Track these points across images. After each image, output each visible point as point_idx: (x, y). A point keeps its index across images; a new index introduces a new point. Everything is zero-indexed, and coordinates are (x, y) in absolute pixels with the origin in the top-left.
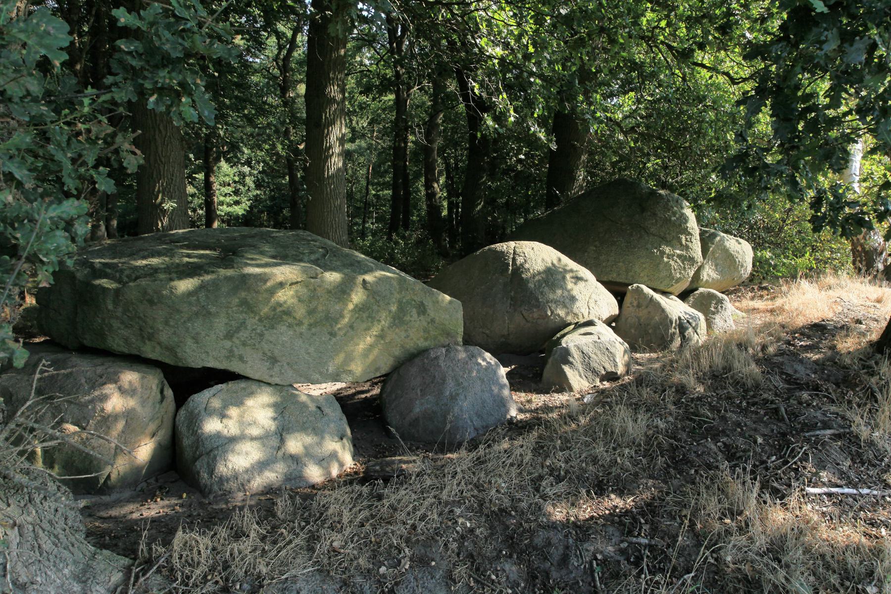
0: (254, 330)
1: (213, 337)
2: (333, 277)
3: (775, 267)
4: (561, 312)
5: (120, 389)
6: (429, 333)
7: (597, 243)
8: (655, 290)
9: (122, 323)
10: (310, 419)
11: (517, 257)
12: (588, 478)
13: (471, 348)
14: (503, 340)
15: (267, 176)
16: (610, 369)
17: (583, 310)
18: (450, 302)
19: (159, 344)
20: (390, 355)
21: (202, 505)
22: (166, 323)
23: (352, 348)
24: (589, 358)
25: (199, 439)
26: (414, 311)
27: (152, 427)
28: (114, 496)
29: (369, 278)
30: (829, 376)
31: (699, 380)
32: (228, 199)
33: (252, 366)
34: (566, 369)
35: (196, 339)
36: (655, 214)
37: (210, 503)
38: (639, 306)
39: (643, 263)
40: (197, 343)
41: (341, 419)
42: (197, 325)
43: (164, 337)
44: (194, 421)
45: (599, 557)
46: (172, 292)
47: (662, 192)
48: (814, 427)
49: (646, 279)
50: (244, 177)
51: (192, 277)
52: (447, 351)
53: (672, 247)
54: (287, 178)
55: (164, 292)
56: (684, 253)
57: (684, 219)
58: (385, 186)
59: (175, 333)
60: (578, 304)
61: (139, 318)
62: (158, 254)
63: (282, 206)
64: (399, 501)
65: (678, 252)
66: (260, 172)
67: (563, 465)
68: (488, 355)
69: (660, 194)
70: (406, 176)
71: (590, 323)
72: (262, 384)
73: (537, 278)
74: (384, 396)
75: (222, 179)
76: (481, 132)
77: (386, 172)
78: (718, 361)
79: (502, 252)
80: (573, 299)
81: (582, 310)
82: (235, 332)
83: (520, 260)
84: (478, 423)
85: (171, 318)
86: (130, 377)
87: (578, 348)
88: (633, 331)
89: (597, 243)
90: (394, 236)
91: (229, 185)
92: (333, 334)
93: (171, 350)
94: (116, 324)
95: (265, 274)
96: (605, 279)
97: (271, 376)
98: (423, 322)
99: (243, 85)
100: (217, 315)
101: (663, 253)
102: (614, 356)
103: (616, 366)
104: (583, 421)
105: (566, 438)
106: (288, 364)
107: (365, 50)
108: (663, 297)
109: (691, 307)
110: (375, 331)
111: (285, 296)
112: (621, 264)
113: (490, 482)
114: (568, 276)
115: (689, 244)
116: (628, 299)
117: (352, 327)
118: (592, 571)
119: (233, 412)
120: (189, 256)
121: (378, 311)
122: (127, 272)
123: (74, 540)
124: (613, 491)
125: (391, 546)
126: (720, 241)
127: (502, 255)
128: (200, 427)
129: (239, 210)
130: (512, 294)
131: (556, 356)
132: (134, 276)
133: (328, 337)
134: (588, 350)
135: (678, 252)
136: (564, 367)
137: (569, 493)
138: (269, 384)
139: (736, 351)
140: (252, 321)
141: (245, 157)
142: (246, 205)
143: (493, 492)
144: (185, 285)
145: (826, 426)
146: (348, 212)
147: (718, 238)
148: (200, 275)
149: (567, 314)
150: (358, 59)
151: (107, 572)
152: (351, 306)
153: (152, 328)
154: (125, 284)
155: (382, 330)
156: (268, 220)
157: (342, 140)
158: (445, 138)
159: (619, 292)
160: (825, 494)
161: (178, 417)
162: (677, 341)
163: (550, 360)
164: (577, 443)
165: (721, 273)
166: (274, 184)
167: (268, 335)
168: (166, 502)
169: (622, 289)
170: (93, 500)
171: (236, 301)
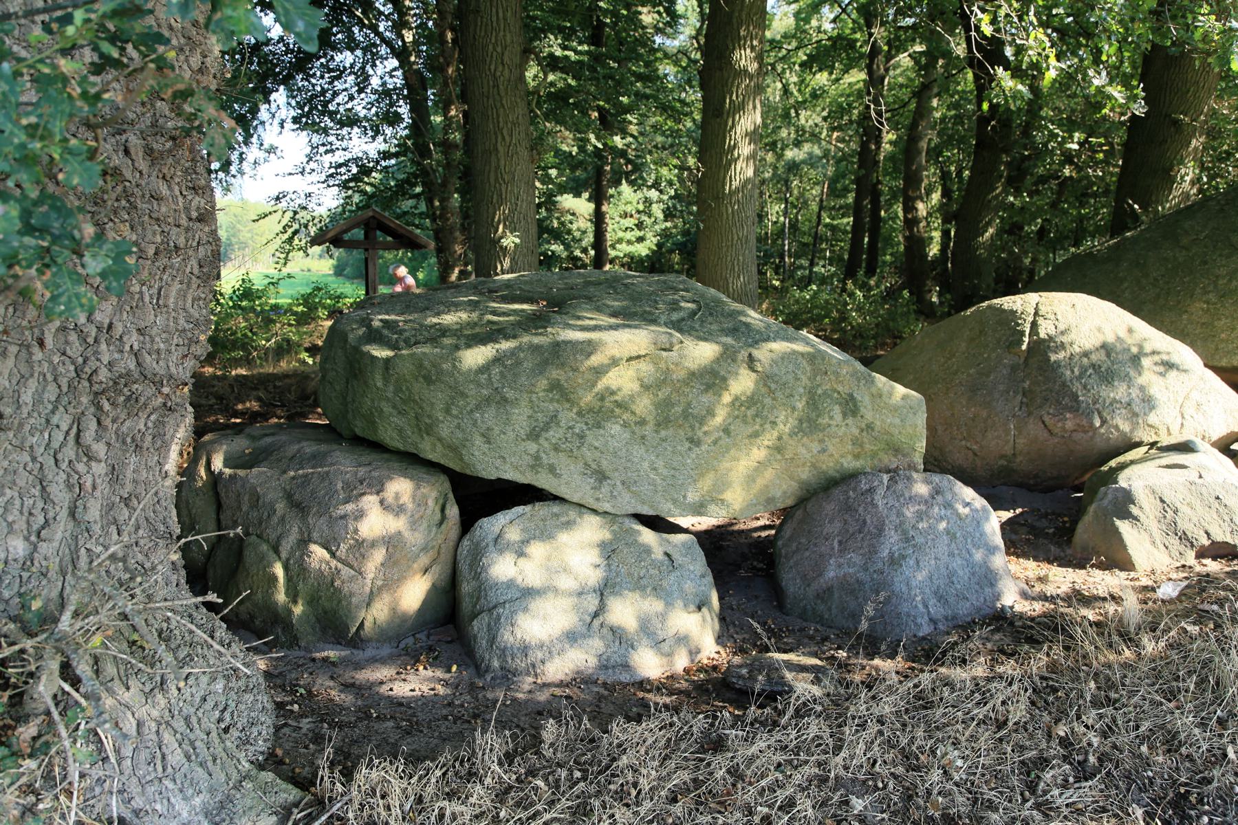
0: (570, 428)
2: (702, 352)
4: (1125, 427)
5: (382, 502)
6: (861, 446)
7: (1212, 297)
9: (394, 407)
10: (652, 572)
11: (1040, 321)
12: (1151, 780)
13: (936, 478)
18: (904, 397)
19: (440, 440)
20: (791, 478)
21: (472, 688)
22: (447, 411)
23: (728, 465)
25: (482, 586)
26: (837, 409)
27: (424, 560)
28: (369, 652)
32: (629, 235)
34: (1123, 526)
37: (483, 688)
40: (489, 442)
41: (703, 576)
42: (489, 417)
43: (445, 430)
46: (454, 366)
51: (485, 344)
55: (444, 366)
58: (844, 211)
59: (458, 426)
61: (414, 401)
64: (751, 760)
67: (1096, 741)
68: (968, 493)
70: (875, 195)
71: (1185, 447)
72: (584, 510)
74: (780, 543)
75: (622, 208)
76: (990, 102)
79: (1013, 312)
80: (1149, 402)
82: (542, 430)
83: (1045, 329)
84: (936, 610)
85: (453, 404)
86: (400, 487)
89: (1212, 297)
92: (695, 442)
93: (454, 449)
94: (387, 409)
96: (1216, 364)
99: (651, 77)
104: (1150, 646)
105: (1108, 679)
106: (623, 483)
107: (826, 10)
110: (769, 438)
111: (622, 380)
113: (933, 752)
114: (1146, 362)
117: (726, 431)
119: (537, 550)
120: (494, 313)
121: (773, 407)
123: (219, 750)
127: (1011, 317)
128: (485, 569)
129: (642, 250)
131: (1106, 502)
132: (413, 340)
133: (687, 445)
136: (1118, 523)
137: (1104, 810)
140: (567, 416)
142: (651, 242)
143: (936, 775)
144: (475, 357)
146: (789, 250)
148: (496, 341)
150: (814, 23)
151: (253, 813)
153: (429, 417)
155: (780, 438)
156: (681, 263)
157: (754, 136)
161: (460, 550)
164: (1132, 694)
167: (590, 437)
168: (429, 673)
170: (343, 653)
171: (543, 383)
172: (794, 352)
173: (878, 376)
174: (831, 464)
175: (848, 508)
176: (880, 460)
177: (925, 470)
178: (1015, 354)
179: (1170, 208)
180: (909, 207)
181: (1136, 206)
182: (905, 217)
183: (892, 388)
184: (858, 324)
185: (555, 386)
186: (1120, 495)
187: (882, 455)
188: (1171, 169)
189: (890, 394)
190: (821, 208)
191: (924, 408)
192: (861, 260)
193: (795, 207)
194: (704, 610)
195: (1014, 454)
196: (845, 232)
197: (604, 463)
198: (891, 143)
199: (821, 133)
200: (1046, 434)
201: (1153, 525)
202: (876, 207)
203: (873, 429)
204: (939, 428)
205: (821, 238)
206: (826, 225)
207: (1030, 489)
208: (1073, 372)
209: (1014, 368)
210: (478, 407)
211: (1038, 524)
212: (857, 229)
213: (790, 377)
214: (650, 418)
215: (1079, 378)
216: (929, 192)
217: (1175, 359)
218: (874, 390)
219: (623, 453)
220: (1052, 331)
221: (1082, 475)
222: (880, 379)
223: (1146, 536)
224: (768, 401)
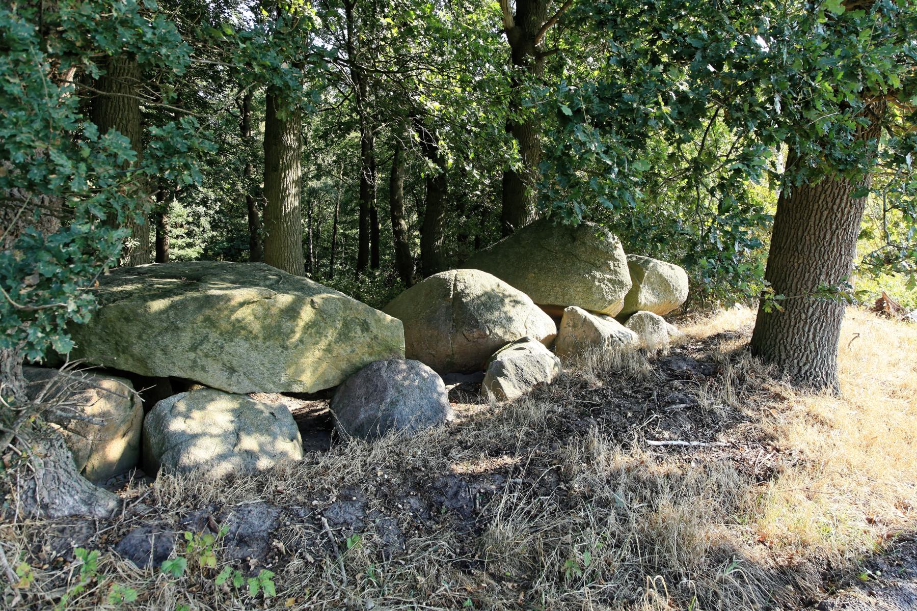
1: (180, 349)
2: (285, 299)
4: (499, 331)
7: (536, 270)
8: (590, 312)
9: (101, 338)
11: (458, 283)
13: (411, 361)
14: (448, 359)
15: (225, 215)
17: (520, 330)
18: (392, 321)
19: (132, 356)
20: (337, 368)
22: (140, 337)
24: (522, 370)
26: (358, 329)
27: (123, 428)
29: (317, 299)
30: (704, 370)
32: (180, 242)
33: (215, 376)
34: (501, 380)
35: (165, 351)
36: (584, 243)
40: (166, 354)
41: (292, 424)
42: (167, 339)
43: (136, 349)
44: (161, 422)
45: (482, 491)
46: (146, 311)
48: (674, 403)
49: (581, 301)
50: (199, 217)
54: (247, 218)
56: (613, 277)
57: (611, 248)
59: (146, 346)
60: (514, 324)
62: (132, 282)
63: (241, 247)
65: (608, 276)
66: (217, 212)
69: (588, 226)
70: (373, 214)
71: (525, 340)
73: (476, 302)
75: (173, 220)
77: (353, 210)
80: (510, 319)
81: (519, 328)
83: (460, 286)
86: (109, 384)
89: (536, 270)
90: (361, 276)
91: (182, 226)
93: (142, 361)
94: (94, 339)
95: (226, 295)
96: (545, 303)
97: (230, 385)
98: (366, 338)
100: (183, 329)
101: (594, 277)
102: (544, 368)
106: (245, 374)
110: (323, 343)
114: (507, 301)
115: (618, 269)
116: (565, 320)
118: (475, 498)
119: (196, 414)
121: (325, 328)
122: (105, 296)
124: (506, 454)
125: (323, 489)
127: (445, 281)
128: (166, 426)
132: (112, 299)
133: (281, 349)
135: (608, 276)
138: (227, 393)
140: (214, 336)
141: (201, 196)
144: (158, 305)
145: (682, 401)
146: (314, 253)
147: (651, 264)
148: (170, 297)
149: (505, 333)
152: (301, 324)
153: (127, 342)
154: (105, 306)
155: (329, 345)
159: (555, 313)
160: (664, 445)
165: (658, 296)
166: (232, 224)
167: (226, 348)
169: (558, 312)
171: (200, 318)
175: (368, 380)
180: (396, 223)
185: (207, 319)
189: (384, 319)
190: (336, 222)
194: (295, 441)
196: (354, 239)
197: (234, 362)
202: (374, 224)
205: (337, 244)
207: (464, 373)
209: (448, 308)
210: (160, 334)
212: (363, 237)
213: (333, 311)
214: (260, 335)
217: (519, 299)
219: (245, 356)
222: (379, 312)
224: (322, 324)
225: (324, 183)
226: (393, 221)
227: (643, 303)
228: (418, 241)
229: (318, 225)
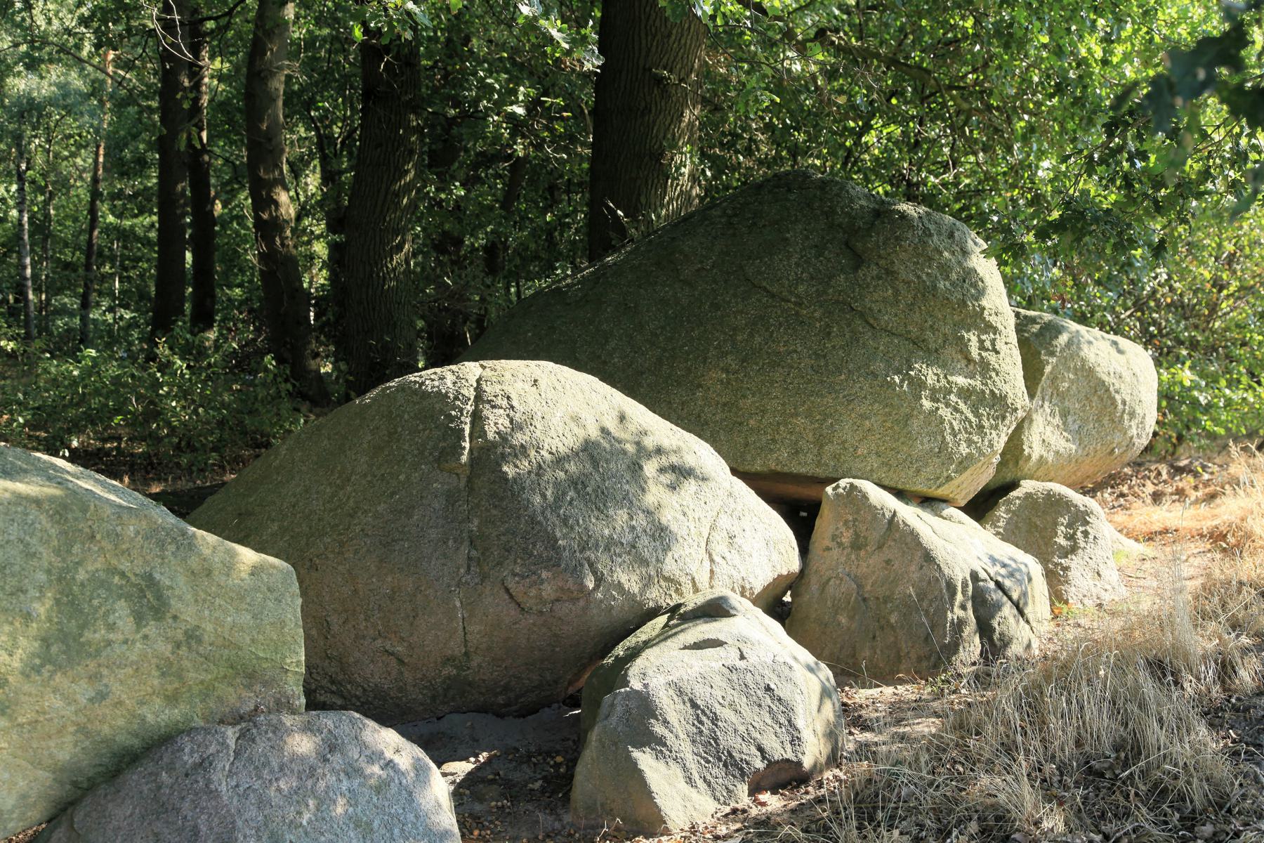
3: (1208, 408)
4: (629, 580)
6: (180, 677)
8: (900, 494)
13: (328, 720)
14: (449, 671)
16: (779, 750)
17: (693, 568)
18: (256, 571)
20: (37, 763)
24: (715, 719)
26: (122, 612)
31: (1050, 792)
34: (645, 759)
36: (890, 273)
38: (857, 545)
39: (863, 417)
47: (906, 207)
49: (874, 462)
52: (242, 736)
53: (943, 366)
56: (977, 383)
57: (971, 283)
58: (140, 202)
60: (676, 551)
65: (961, 381)
68: (388, 740)
69: (903, 216)
71: (716, 610)
78: (1102, 725)
80: (661, 535)
83: (496, 422)
87: (680, 692)
88: (843, 620)
96: (758, 467)
102: (788, 709)
103: (796, 741)
108: (927, 516)
109: (1005, 538)
112: (800, 420)
114: (650, 468)
115: (991, 358)
116: (825, 525)
126: (1069, 344)
130: (474, 525)
131: (614, 719)
134: (713, 694)
135: (961, 381)
136: (636, 754)
139: (1149, 687)
146: (35, 276)
147: (1063, 339)
149: (647, 582)
158: (310, 65)
162: (972, 648)
163: (594, 736)
165: (1079, 435)
169: (806, 492)
172: (20, 498)
173: (201, 533)
174: (121, 722)
175: (161, 808)
176: (220, 699)
177: (312, 705)
178: (450, 471)
179: (667, 215)
180: (263, 201)
181: (620, 212)
182: (257, 219)
183: (233, 555)
184: (184, 424)
186: (632, 704)
187: (223, 689)
188: (662, 155)
190: (95, 195)
191: (295, 588)
192: (182, 300)
193: (42, 190)
195: (466, 654)
196: (147, 242)
198: (221, 77)
199: (78, 47)
200: (513, 611)
201: (686, 749)
203: (199, 641)
204: (335, 620)
205: (100, 254)
206: (108, 229)
208: (544, 496)
209: (451, 497)
211: (516, 776)
215: (556, 506)
216: (297, 170)
217: (690, 461)
218: (194, 562)
220: (504, 423)
221: (578, 676)
222: (207, 539)
223: (676, 770)
225: (60, 86)
226: (254, 195)
227: (1035, 457)
228: (320, 248)
229: (46, 203)
